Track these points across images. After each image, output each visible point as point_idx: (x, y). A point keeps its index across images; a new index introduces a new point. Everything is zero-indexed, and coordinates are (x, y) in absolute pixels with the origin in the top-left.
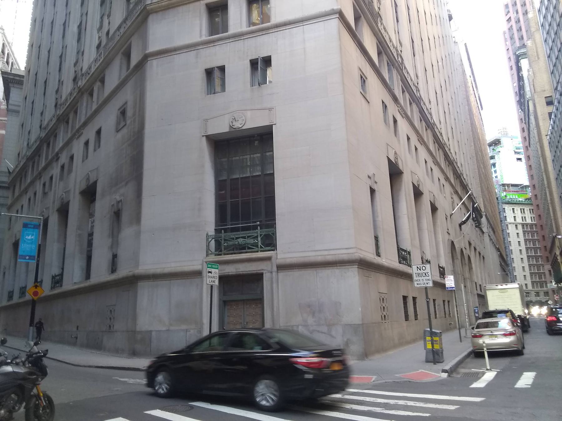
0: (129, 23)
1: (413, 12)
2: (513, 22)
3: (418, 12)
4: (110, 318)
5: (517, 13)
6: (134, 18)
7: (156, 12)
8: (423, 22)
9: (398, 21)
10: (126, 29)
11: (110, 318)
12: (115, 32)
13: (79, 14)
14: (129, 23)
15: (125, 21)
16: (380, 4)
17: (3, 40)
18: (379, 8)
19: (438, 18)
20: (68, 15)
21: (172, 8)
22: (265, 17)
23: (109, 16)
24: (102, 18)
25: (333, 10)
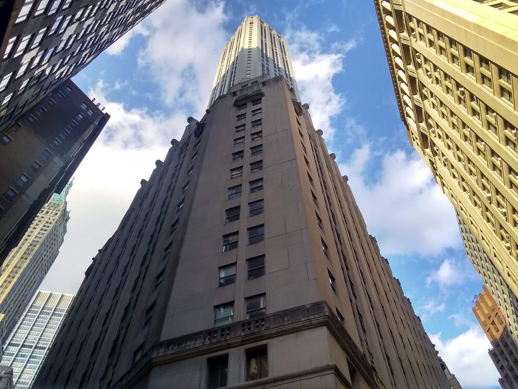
0: (132, 375)
1: (406, 363)
2: (507, 370)
3: (410, 363)
4: (50, 242)
5: (507, 361)
6: (138, 370)
7: (160, 365)
8: (417, 374)
9: (392, 373)
10: (128, 380)
11: (50, 242)
12: (117, 383)
13: (87, 363)
14: (132, 375)
15: (129, 372)
16: (373, 358)
17: (7, 385)
18: (372, 362)
19: (431, 368)
20: (76, 364)
21: (175, 361)
22: (263, 371)
23: (114, 367)
24: (107, 368)
25: (328, 365)
